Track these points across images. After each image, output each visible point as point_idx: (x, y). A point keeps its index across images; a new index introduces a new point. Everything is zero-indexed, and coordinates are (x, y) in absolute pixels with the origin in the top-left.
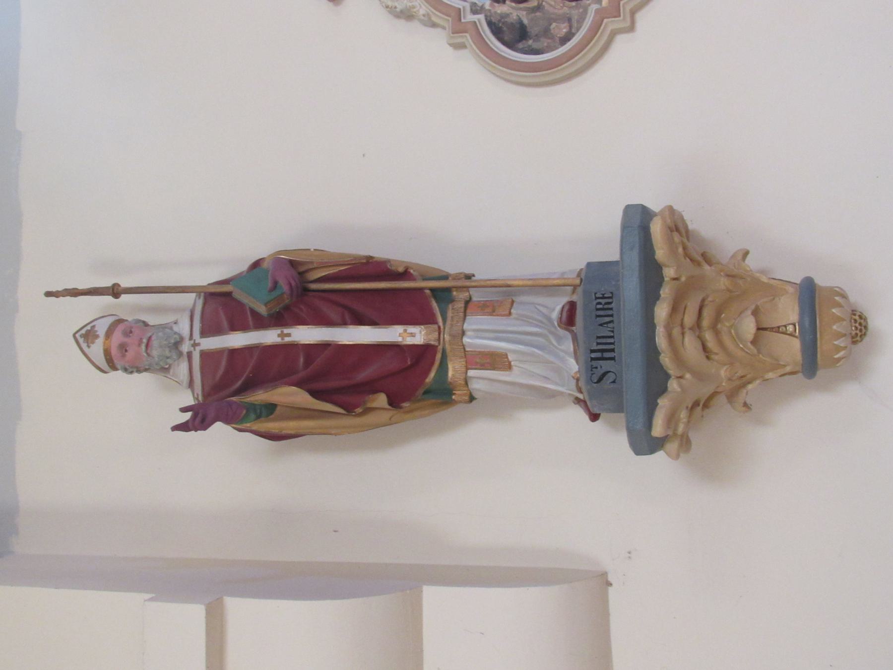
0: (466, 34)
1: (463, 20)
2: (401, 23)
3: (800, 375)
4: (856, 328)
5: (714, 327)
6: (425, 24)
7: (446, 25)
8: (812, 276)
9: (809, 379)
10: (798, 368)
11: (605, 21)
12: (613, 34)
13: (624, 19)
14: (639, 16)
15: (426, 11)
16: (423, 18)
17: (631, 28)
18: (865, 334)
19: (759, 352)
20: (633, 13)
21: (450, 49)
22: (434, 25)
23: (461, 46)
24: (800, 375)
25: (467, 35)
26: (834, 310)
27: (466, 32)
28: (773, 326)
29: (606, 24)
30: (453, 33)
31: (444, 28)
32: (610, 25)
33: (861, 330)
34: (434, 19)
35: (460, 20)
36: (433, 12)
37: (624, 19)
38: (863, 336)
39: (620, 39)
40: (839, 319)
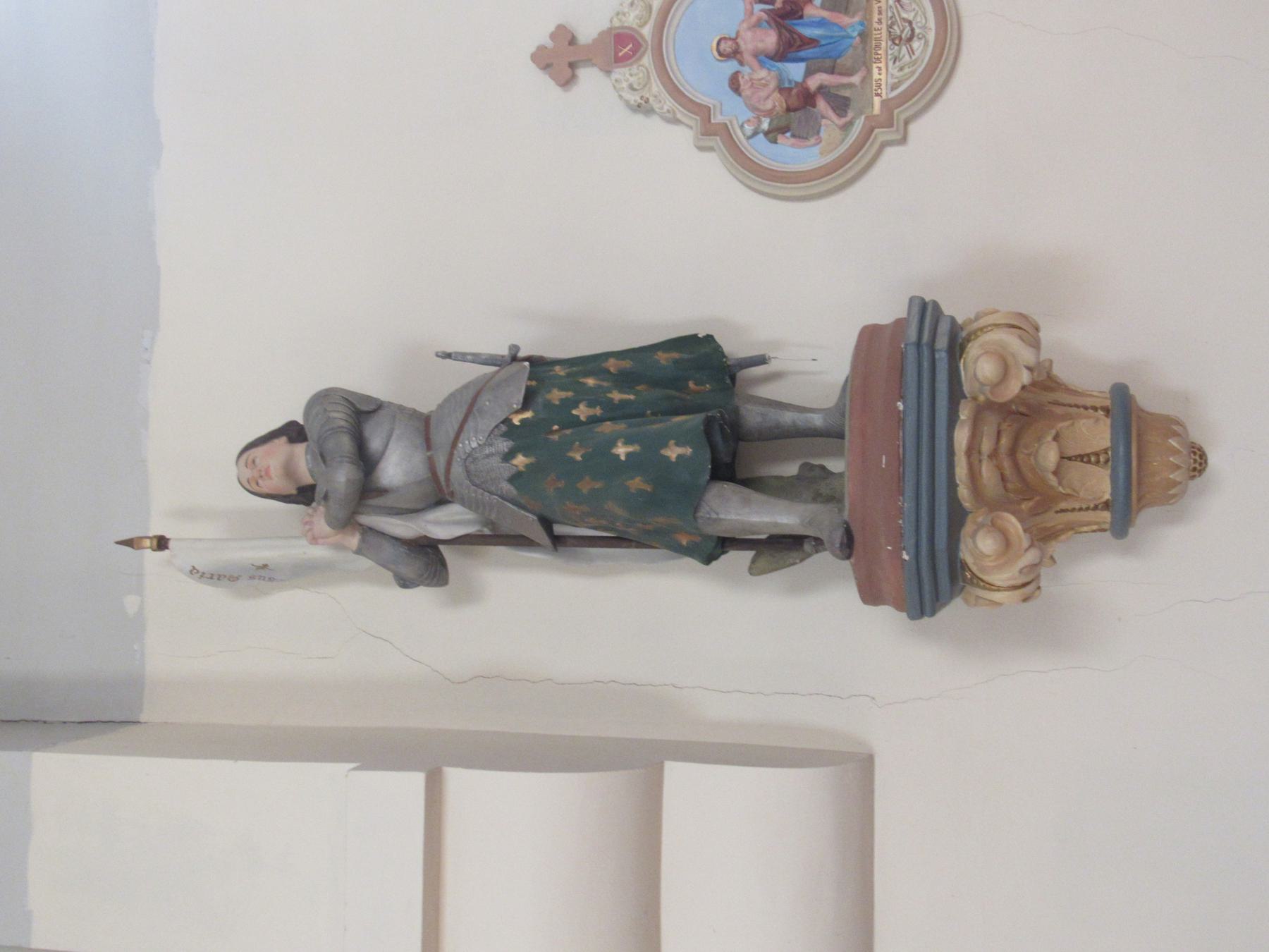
0: (715, 137)
1: (713, 121)
2: (639, 118)
3: (1108, 534)
4: (1195, 461)
5: (1013, 452)
6: (668, 121)
7: (692, 123)
8: (1125, 540)
9: (1117, 538)
10: (1107, 526)
11: (877, 131)
12: (884, 146)
13: (897, 130)
14: (913, 128)
15: (670, 107)
16: (667, 115)
17: (904, 140)
18: (1204, 469)
19: (1060, 483)
20: (907, 123)
21: (695, 150)
22: (676, 121)
23: (711, 149)
24: (1108, 534)
25: (718, 138)
26: (1171, 459)
27: (717, 135)
28: (1088, 451)
29: (876, 135)
30: (703, 135)
31: (691, 128)
32: (881, 135)
33: (1201, 464)
34: (679, 116)
35: (710, 121)
36: (678, 109)
37: (897, 130)
38: (1201, 472)
39: (890, 152)
40: (1175, 452)
